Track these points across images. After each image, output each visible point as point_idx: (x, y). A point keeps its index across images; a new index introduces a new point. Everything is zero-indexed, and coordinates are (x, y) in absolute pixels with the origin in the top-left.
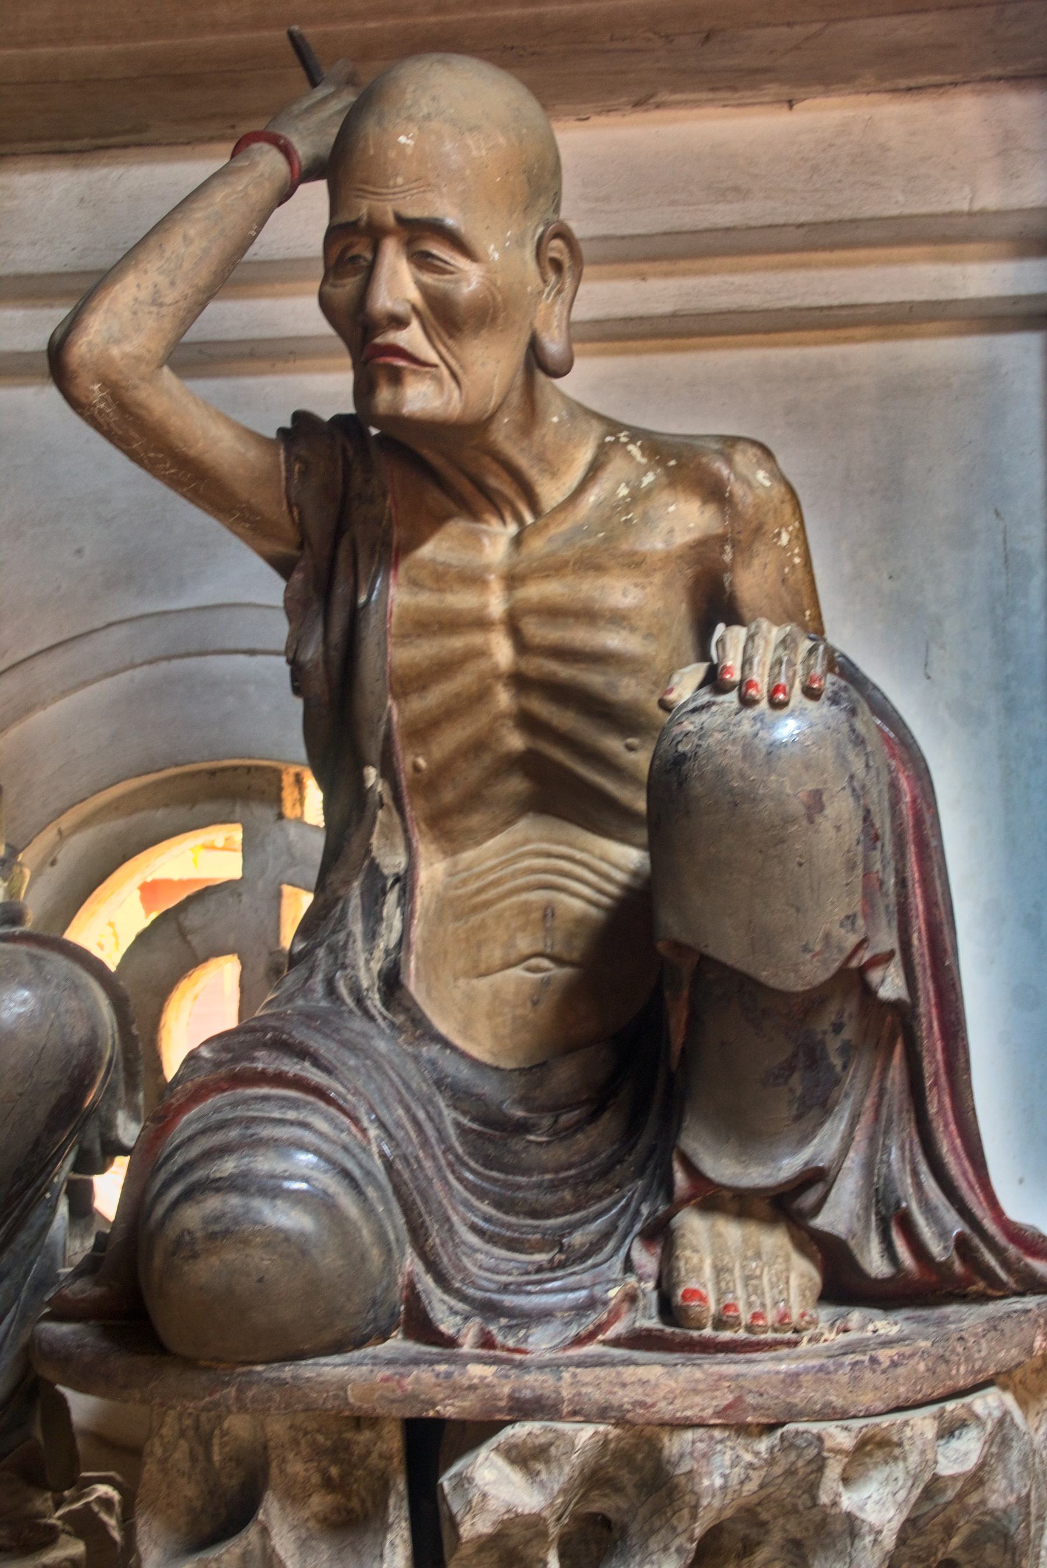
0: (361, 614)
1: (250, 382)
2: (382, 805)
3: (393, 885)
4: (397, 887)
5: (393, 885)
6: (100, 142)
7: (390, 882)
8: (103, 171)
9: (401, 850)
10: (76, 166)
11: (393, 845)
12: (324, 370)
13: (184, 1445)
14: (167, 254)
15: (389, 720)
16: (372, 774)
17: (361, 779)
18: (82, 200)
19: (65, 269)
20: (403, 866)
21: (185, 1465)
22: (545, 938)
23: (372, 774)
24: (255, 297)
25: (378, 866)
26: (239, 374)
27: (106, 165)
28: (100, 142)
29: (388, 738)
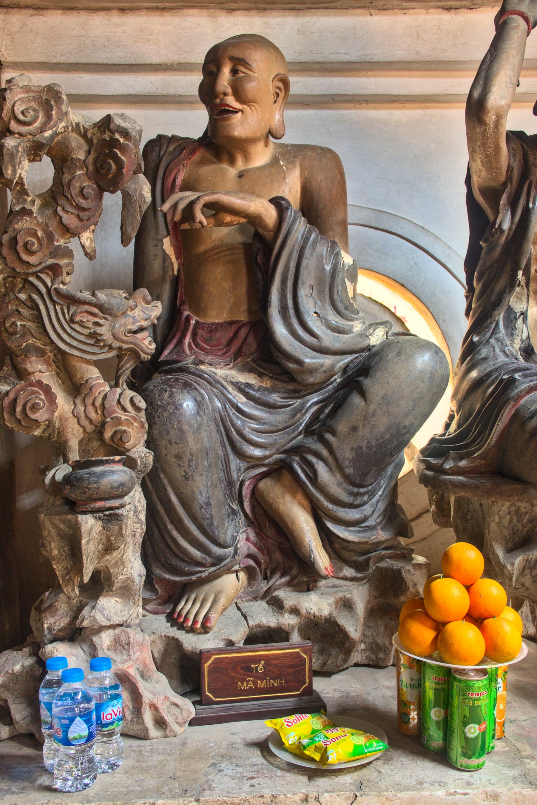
0: (532, 211)
1: (345, 112)
2: (519, 284)
3: (520, 316)
4: (522, 316)
5: (520, 316)
6: (312, 6)
7: (518, 315)
8: (308, 19)
9: (525, 303)
10: (297, 16)
11: (521, 301)
12: (375, 109)
13: (508, 517)
14: (510, 63)
15: (531, 253)
16: (520, 273)
17: (516, 275)
18: (299, 31)
19: (293, 61)
20: (525, 309)
21: (506, 524)
22: (371, 334)
23: (520, 273)
24: (360, 76)
25: (512, 309)
26: (340, 109)
27: (309, 16)
28: (312, 6)
29: (529, 259)
